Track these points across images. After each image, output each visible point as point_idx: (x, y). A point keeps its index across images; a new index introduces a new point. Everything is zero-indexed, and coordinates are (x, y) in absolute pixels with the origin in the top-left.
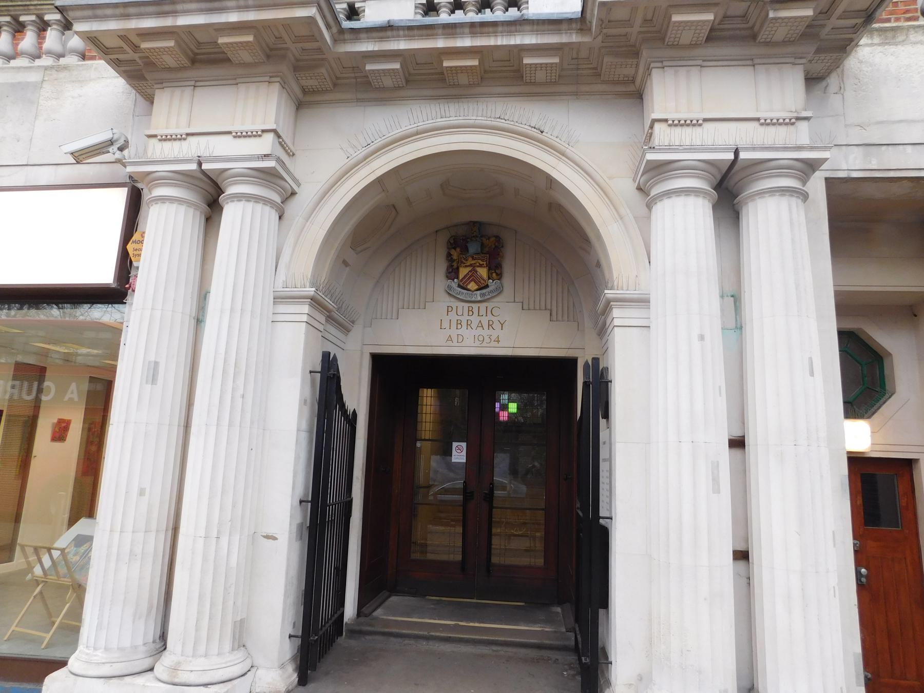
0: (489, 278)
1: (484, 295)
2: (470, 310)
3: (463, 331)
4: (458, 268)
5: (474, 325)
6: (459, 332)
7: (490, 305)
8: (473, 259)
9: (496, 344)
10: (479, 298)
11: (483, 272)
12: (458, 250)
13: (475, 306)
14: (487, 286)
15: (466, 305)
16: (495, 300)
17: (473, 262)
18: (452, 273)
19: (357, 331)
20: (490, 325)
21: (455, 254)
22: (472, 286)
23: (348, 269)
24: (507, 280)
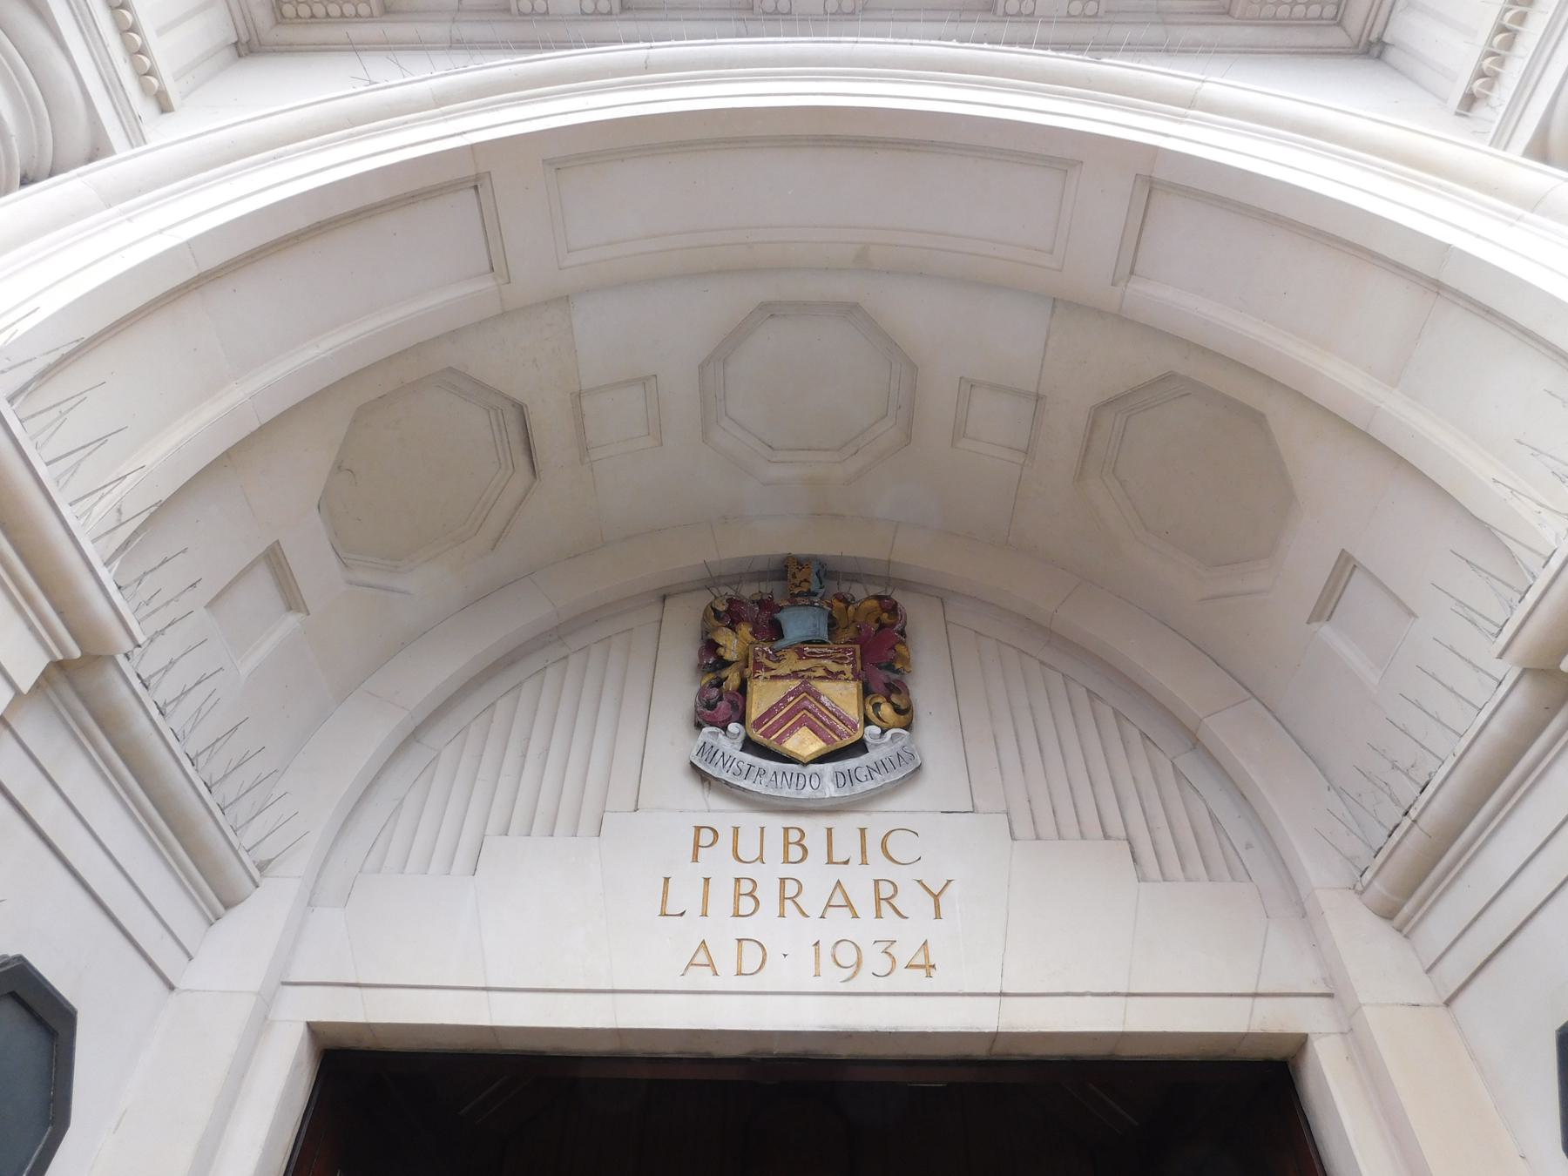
0: (867, 722)
1: (851, 777)
2: (795, 846)
3: (764, 924)
4: (743, 689)
5: (813, 900)
6: (747, 928)
7: (876, 822)
8: (801, 655)
10: (830, 791)
11: (842, 696)
12: (745, 630)
13: (814, 828)
14: (860, 747)
15: (775, 824)
16: (894, 803)
17: (803, 665)
18: (719, 703)
19: (263, 917)
20: (884, 900)
21: (732, 644)
22: (804, 743)
23: (293, 620)
24: (934, 738)
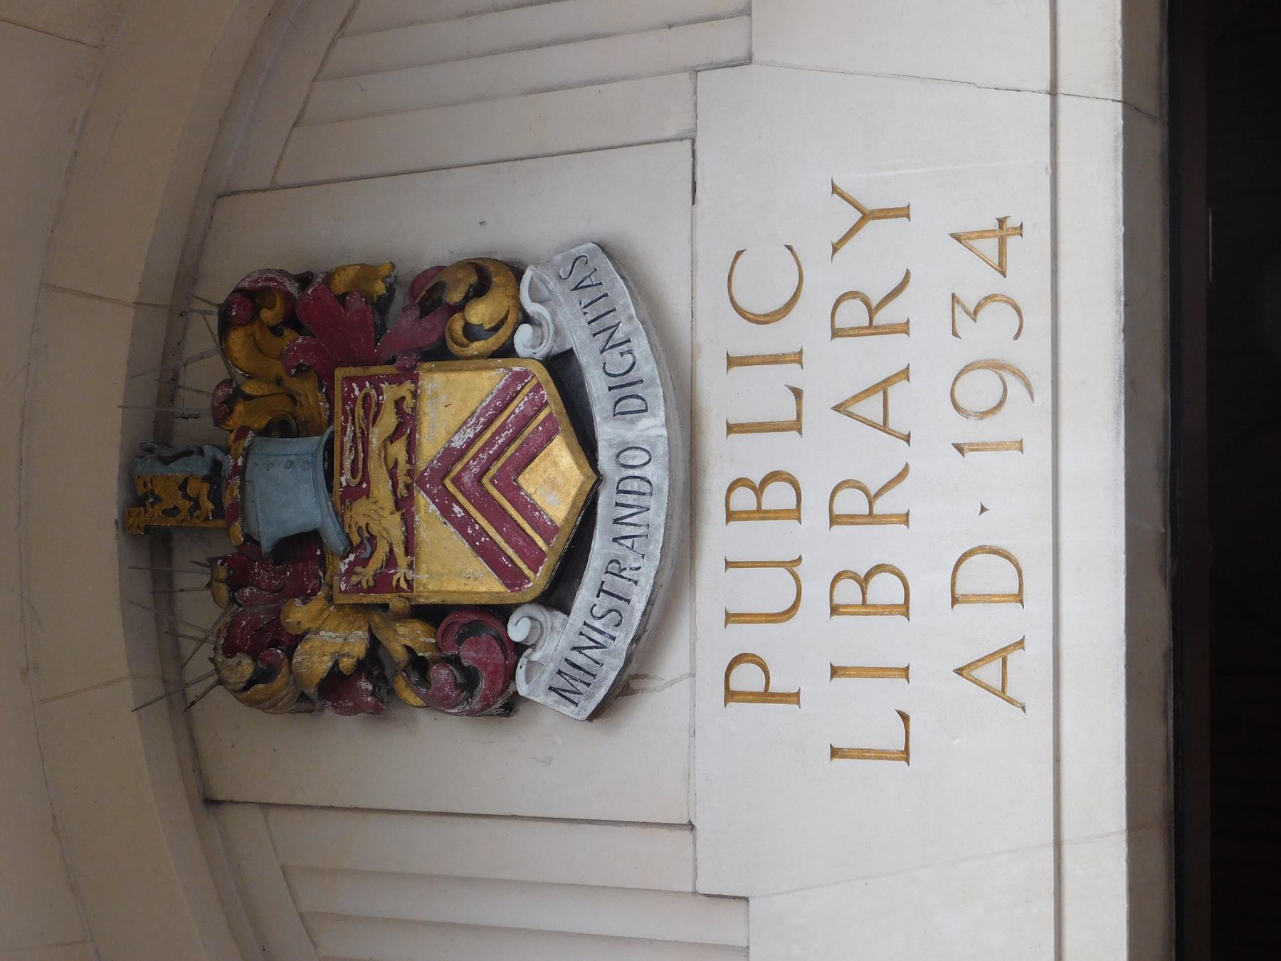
0: (507, 351)
1: (625, 387)
2: (764, 499)
4: (432, 614)
5: (872, 458)
6: (930, 586)
7: (714, 334)
9: (1028, 254)
10: (653, 426)
11: (451, 403)
12: (299, 614)
13: (726, 459)
14: (562, 366)
15: (719, 540)
16: (677, 300)
17: (382, 488)
18: (467, 664)
20: (873, 317)
21: (330, 643)
22: (553, 481)
24: (537, 217)
